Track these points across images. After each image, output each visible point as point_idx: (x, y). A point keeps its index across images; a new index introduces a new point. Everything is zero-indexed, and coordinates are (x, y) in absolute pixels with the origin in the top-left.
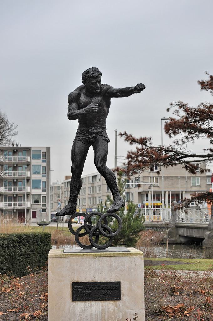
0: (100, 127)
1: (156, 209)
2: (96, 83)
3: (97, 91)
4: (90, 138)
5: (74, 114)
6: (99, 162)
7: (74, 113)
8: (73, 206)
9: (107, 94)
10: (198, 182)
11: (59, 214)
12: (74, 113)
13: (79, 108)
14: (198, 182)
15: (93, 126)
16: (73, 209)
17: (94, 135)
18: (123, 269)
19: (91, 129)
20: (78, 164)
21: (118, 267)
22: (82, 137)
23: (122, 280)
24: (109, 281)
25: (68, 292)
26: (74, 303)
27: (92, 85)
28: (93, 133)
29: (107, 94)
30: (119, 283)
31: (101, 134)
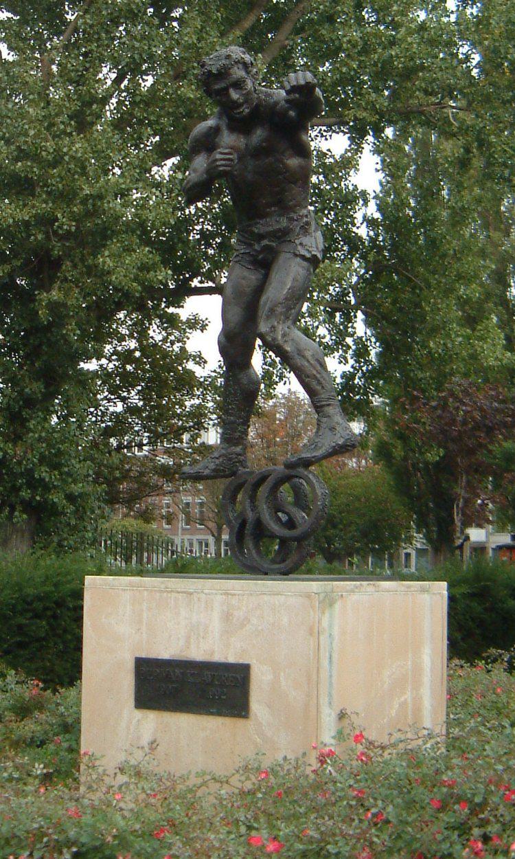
2: (226, 89)
3: (239, 113)
17: (265, 242)
24: (222, 660)
25: (127, 683)
26: (139, 714)
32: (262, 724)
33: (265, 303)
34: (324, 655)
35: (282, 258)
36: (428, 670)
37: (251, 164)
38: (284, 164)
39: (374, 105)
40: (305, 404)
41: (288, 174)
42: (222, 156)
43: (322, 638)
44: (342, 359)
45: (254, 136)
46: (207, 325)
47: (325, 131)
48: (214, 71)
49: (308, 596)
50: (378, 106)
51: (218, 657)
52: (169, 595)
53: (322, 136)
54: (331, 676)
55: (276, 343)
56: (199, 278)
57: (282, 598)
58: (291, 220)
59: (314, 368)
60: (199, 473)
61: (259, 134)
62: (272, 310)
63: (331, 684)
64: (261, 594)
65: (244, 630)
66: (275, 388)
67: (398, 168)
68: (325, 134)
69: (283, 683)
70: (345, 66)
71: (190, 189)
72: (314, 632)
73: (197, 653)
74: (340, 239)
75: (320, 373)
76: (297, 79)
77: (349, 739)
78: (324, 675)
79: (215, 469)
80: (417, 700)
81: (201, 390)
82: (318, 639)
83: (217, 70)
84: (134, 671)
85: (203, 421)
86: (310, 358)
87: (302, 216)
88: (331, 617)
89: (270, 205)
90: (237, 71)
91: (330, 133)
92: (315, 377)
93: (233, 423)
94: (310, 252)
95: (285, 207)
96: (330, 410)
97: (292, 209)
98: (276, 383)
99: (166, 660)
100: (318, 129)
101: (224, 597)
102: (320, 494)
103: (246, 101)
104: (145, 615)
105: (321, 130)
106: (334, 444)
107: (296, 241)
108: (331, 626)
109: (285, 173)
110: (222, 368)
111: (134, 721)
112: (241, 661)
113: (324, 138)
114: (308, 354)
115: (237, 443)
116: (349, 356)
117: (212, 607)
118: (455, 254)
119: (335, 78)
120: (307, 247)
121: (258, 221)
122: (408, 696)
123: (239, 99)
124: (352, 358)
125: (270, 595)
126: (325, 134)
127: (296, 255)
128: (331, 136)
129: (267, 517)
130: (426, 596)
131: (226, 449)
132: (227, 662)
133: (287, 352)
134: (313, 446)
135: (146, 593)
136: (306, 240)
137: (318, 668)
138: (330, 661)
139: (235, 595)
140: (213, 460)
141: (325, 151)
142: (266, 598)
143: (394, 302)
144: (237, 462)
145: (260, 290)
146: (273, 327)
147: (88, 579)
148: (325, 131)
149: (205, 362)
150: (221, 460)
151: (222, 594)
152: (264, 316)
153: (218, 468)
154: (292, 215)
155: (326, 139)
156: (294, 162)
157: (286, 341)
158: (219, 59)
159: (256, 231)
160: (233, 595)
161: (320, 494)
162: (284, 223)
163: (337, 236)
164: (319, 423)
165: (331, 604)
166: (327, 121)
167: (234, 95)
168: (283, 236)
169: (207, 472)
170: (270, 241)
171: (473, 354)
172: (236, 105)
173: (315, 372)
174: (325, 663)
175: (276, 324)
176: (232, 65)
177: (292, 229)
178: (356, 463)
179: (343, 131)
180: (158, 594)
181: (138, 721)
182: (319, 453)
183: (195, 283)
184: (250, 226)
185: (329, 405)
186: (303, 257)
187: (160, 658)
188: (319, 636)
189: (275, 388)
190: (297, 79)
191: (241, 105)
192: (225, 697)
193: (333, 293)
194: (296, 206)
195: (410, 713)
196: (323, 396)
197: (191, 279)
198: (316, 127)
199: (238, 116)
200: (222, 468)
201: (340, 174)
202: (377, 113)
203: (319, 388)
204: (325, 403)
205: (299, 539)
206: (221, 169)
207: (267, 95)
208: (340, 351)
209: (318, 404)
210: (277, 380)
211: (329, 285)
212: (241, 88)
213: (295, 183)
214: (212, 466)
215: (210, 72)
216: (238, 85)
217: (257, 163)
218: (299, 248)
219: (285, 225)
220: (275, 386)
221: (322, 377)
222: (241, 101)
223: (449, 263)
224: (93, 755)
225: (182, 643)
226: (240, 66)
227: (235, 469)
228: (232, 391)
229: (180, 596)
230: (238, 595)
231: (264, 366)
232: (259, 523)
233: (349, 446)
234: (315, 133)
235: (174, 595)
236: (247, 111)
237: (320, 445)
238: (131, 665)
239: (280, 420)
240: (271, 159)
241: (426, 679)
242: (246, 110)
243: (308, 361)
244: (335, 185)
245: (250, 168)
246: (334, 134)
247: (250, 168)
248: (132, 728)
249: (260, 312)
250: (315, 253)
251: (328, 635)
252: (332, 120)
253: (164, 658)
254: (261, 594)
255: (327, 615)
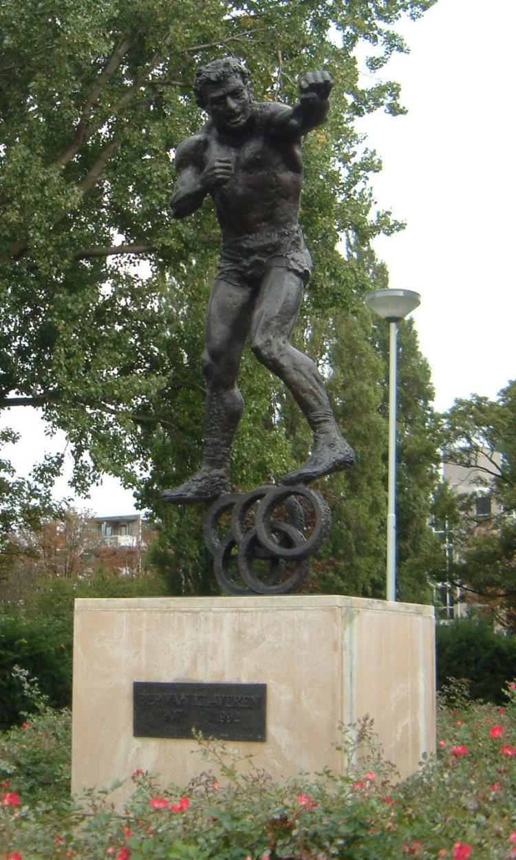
0: (273, 230)
2: (224, 98)
3: (235, 123)
17: (256, 257)
18: (277, 646)
20: (332, 370)
21: (260, 641)
23: (271, 681)
24: (235, 681)
25: (125, 711)
26: (138, 743)
32: (280, 747)
33: (260, 318)
34: (346, 673)
35: (275, 271)
36: (423, 695)
37: (242, 177)
38: (277, 178)
39: (180, 235)
40: (82, 518)
41: (280, 188)
42: (221, 164)
43: (344, 653)
44: (143, 467)
45: (248, 148)
46: (18, 438)
47: (133, 258)
48: (213, 78)
49: (332, 610)
50: (183, 235)
51: (229, 679)
52: (172, 615)
53: (131, 262)
54: (352, 695)
55: (273, 357)
56: (17, 390)
57: (302, 614)
58: (283, 235)
59: (311, 382)
60: (182, 495)
61: (252, 148)
62: (267, 324)
63: (351, 703)
64: (277, 610)
65: (259, 648)
66: (88, 490)
67: (200, 292)
68: (133, 260)
69: (305, 703)
70: (154, 198)
71: (180, 201)
72: (336, 647)
73: (205, 674)
74: (143, 357)
75: (317, 389)
76: (315, 77)
77: (369, 761)
78: (347, 694)
79: (197, 492)
80: (415, 724)
81: (10, 494)
82: (342, 655)
83: (217, 77)
84: (132, 697)
85: (11, 523)
86: (306, 373)
87: (293, 232)
88: (351, 634)
89: (260, 220)
90: (235, 79)
91: (138, 260)
92: (313, 394)
93: (217, 444)
94: (302, 267)
95: (274, 220)
96: (326, 426)
97: (283, 224)
98: (89, 485)
99: (169, 684)
100: (128, 256)
101: (235, 614)
102: (323, 511)
103: (243, 111)
104: (144, 637)
105: (129, 256)
106: (334, 460)
107: (288, 256)
108: (351, 643)
109: (278, 186)
110: (37, 472)
111: (133, 751)
112: (255, 682)
113: (132, 264)
114: (304, 369)
115: (219, 465)
116: (148, 463)
117: (221, 627)
118: (248, 371)
119: (145, 209)
120: (299, 263)
121: (247, 236)
122: (408, 720)
123: (236, 108)
124: (151, 466)
125: (288, 610)
126: (133, 260)
127: (289, 270)
128: (138, 263)
129: (264, 536)
130: (419, 619)
131: (209, 472)
132: (239, 682)
133: (282, 366)
134: (313, 462)
135: (145, 614)
136: (297, 256)
137: (342, 685)
138: (351, 679)
139: (247, 612)
140: (195, 483)
141: (133, 276)
142: (284, 614)
143: (192, 415)
144: (220, 485)
145: (248, 307)
146: (269, 341)
147: (78, 602)
148: (133, 258)
149: (14, 471)
150: (204, 482)
151: (232, 612)
152: (259, 331)
153: (201, 490)
154: (283, 230)
155: (135, 265)
156: (287, 176)
157: (282, 355)
158: (217, 67)
159: (246, 246)
160: (246, 612)
161: (323, 511)
162: (275, 238)
163: (139, 354)
164: (316, 439)
165: (351, 620)
166: (137, 248)
167: (233, 104)
168: (274, 251)
169: (189, 494)
170: (260, 256)
171: (261, 462)
172: (232, 114)
173: (311, 387)
174: (347, 680)
175: (271, 337)
176: (231, 73)
177: (282, 244)
178: (129, 570)
179: (149, 258)
180: (159, 614)
181: (138, 749)
182: (319, 469)
183: (12, 395)
184: (238, 241)
185: (326, 421)
186: (296, 272)
187: (162, 681)
188: (342, 652)
189: (88, 490)
190: (315, 77)
191: (238, 114)
192: (238, 721)
193: (136, 406)
194: (287, 221)
195: (410, 738)
196: (320, 412)
197: (7, 392)
198: (125, 254)
199: (233, 126)
200: (204, 491)
201: (147, 297)
202: (182, 241)
203: (315, 403)
204: (322, 419)
205: (298, 559)
206: (220, 176)
207: (261, 107)
208: (141, 459)
209: (316, 420)
210: (90, 481)
211: (133, 397)
212: (239, 98)
213: (286, 198)
214: (194, 489)
215: (208, 80)
216: (236, 94)
217: (250, 176)
218: (292, 262)
219: (276, 240)
220: (88, 487)
221: (319, 392)
222: (238, 110)
223: (242, 379)
224: (147, 774)
225: (187, 665)
226: (238, 75)
227: (217, 492)
228: (216, 412)
229: (184, 616)
230: (252, 612)
231: (76, 471)
232: (255, 542)
233: (348, 462)
234: (125, 259)
235: (178, 614)
236: (243, 121)
237: (320, 461)
238: (128, 691)
239: (60, 532)
240: (263, 173)
241: (421, 704)
242: (242, 120)
243: (305, 376)
244: (142, 307)
245: (241, 181)
246: (141, 261)
247: (241, 181)
248: (130, 757)
249: (254, 326)
250: (307, 269)
251: (349, 651)
252: (142, 248)
253: (167, 682)
254: (277, 610)
255: (348, 629)
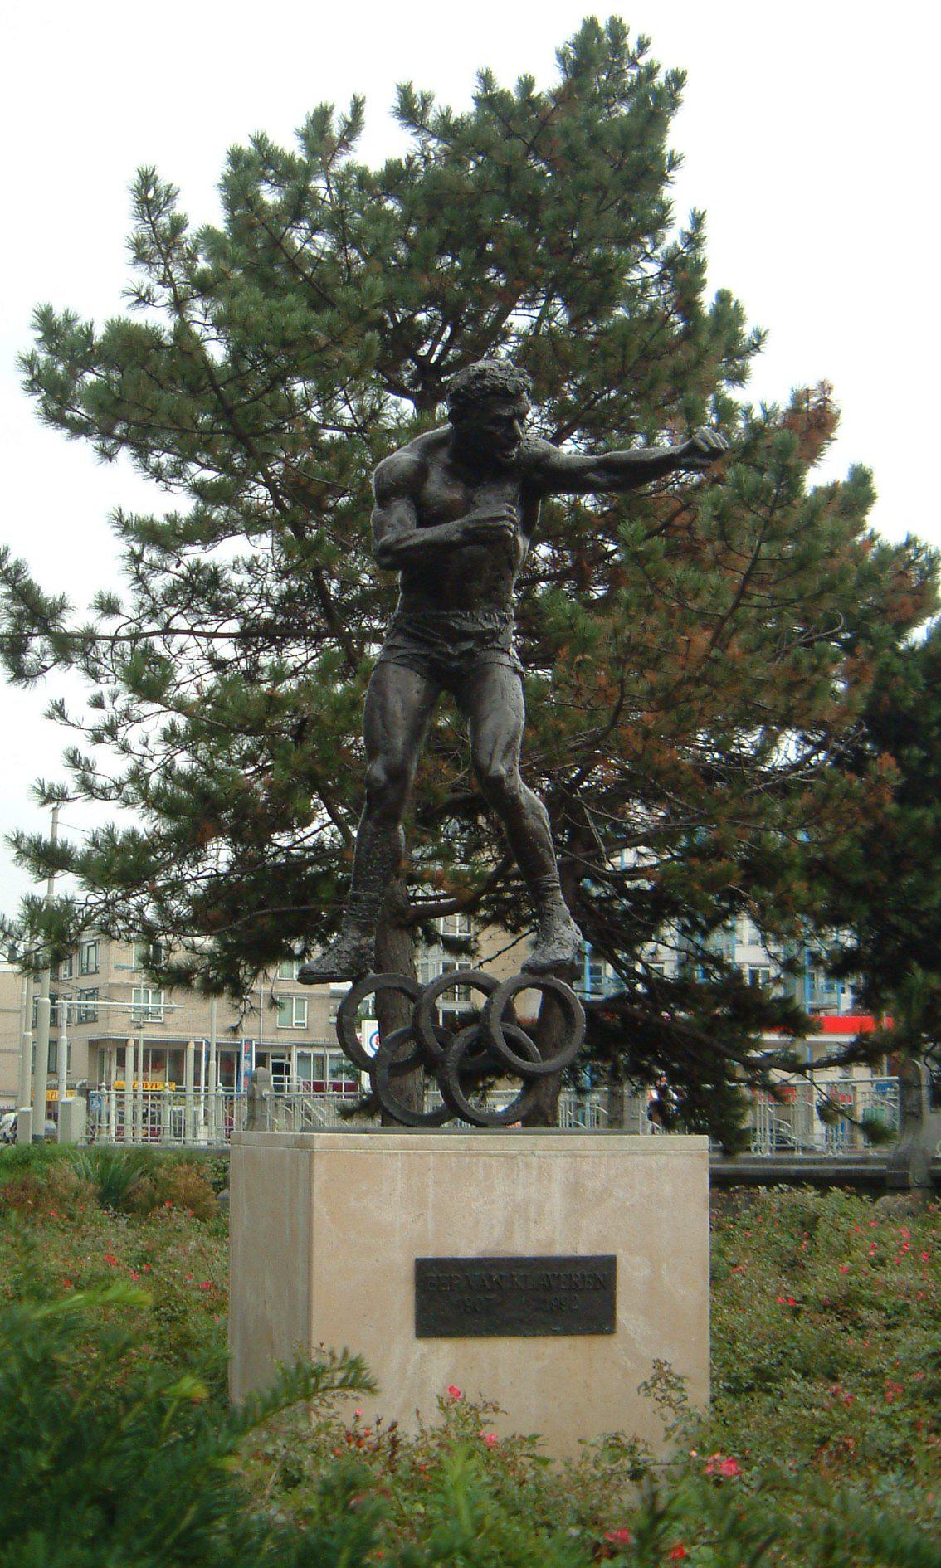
1: (150, 1102)
4: (450, 657)
5: (411, 542)
6: (498, 755)
7: (411, 537)
8: (364, 942)
9: (538, 477)
10: (300, 1015)
11: (312, 973)
12: (411, 537)
13: (422, 523)
14: (300, 1015)
15: (466, 604)
16: (363, 955)
17: (469, 645)
19: (460, 616)
22: (415, 651)
27: (491, 428)
28: (466, 636)
29: (538, 477)
30: (606, 1266)
31: (497, 645)
